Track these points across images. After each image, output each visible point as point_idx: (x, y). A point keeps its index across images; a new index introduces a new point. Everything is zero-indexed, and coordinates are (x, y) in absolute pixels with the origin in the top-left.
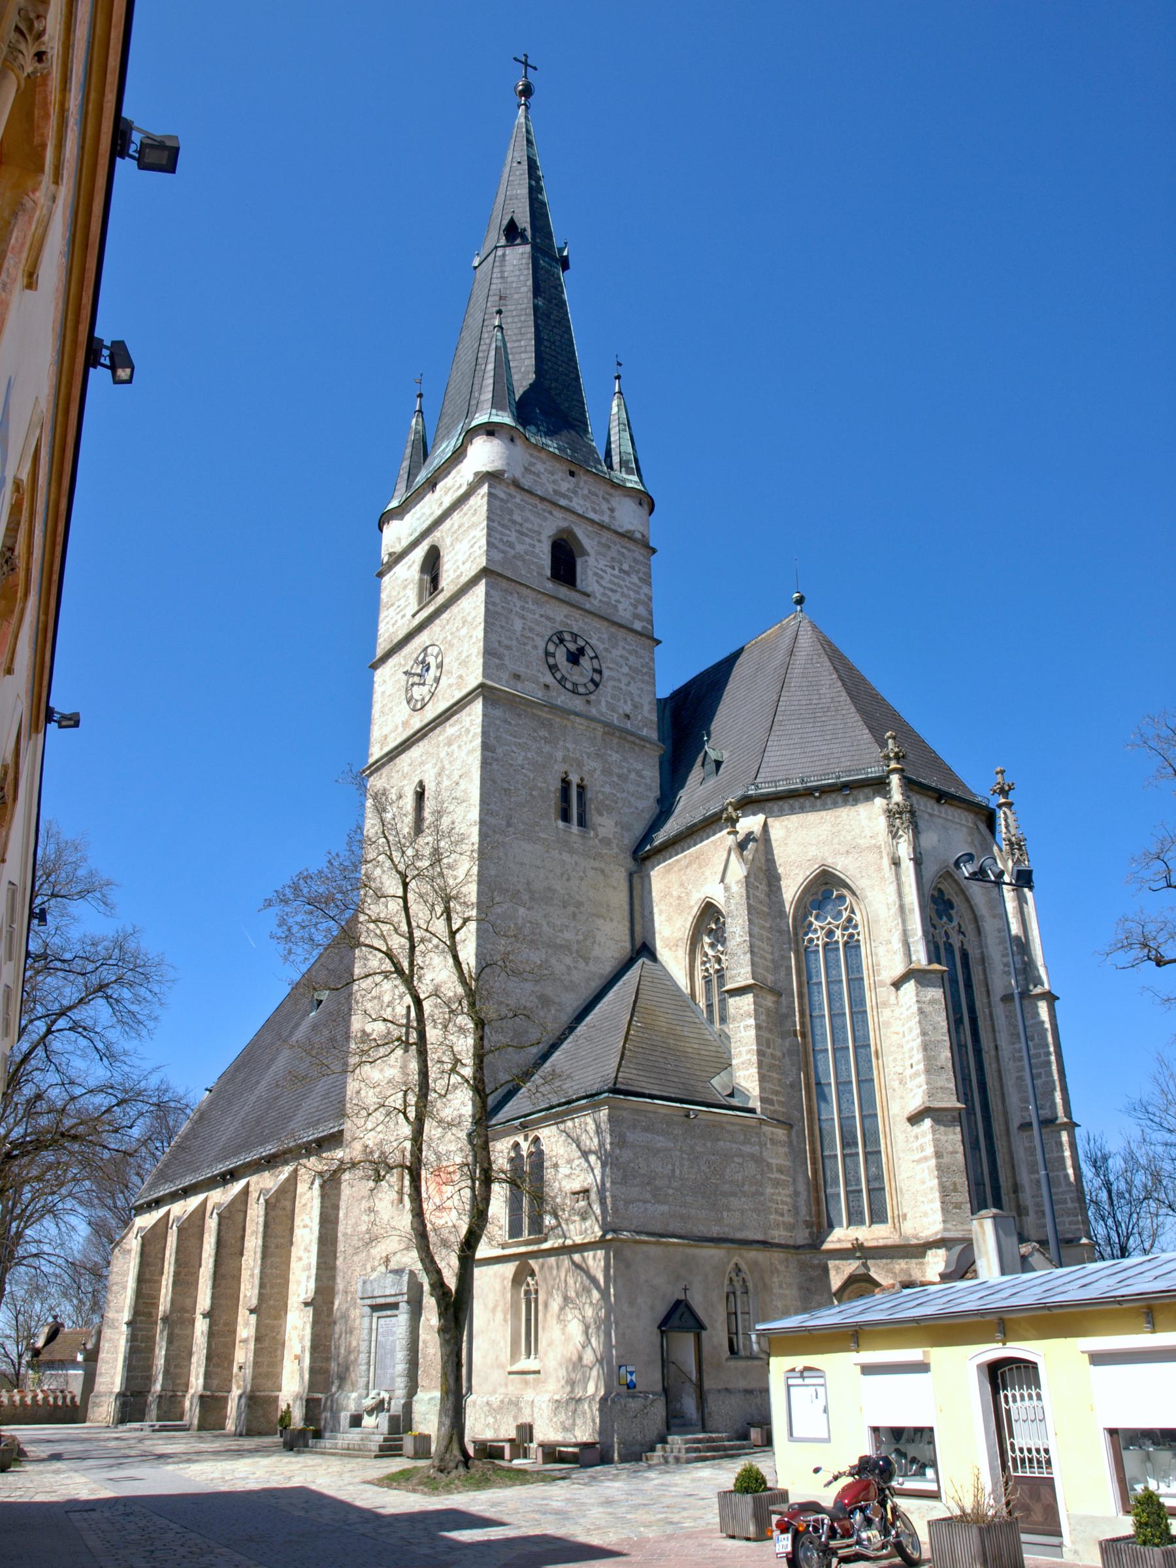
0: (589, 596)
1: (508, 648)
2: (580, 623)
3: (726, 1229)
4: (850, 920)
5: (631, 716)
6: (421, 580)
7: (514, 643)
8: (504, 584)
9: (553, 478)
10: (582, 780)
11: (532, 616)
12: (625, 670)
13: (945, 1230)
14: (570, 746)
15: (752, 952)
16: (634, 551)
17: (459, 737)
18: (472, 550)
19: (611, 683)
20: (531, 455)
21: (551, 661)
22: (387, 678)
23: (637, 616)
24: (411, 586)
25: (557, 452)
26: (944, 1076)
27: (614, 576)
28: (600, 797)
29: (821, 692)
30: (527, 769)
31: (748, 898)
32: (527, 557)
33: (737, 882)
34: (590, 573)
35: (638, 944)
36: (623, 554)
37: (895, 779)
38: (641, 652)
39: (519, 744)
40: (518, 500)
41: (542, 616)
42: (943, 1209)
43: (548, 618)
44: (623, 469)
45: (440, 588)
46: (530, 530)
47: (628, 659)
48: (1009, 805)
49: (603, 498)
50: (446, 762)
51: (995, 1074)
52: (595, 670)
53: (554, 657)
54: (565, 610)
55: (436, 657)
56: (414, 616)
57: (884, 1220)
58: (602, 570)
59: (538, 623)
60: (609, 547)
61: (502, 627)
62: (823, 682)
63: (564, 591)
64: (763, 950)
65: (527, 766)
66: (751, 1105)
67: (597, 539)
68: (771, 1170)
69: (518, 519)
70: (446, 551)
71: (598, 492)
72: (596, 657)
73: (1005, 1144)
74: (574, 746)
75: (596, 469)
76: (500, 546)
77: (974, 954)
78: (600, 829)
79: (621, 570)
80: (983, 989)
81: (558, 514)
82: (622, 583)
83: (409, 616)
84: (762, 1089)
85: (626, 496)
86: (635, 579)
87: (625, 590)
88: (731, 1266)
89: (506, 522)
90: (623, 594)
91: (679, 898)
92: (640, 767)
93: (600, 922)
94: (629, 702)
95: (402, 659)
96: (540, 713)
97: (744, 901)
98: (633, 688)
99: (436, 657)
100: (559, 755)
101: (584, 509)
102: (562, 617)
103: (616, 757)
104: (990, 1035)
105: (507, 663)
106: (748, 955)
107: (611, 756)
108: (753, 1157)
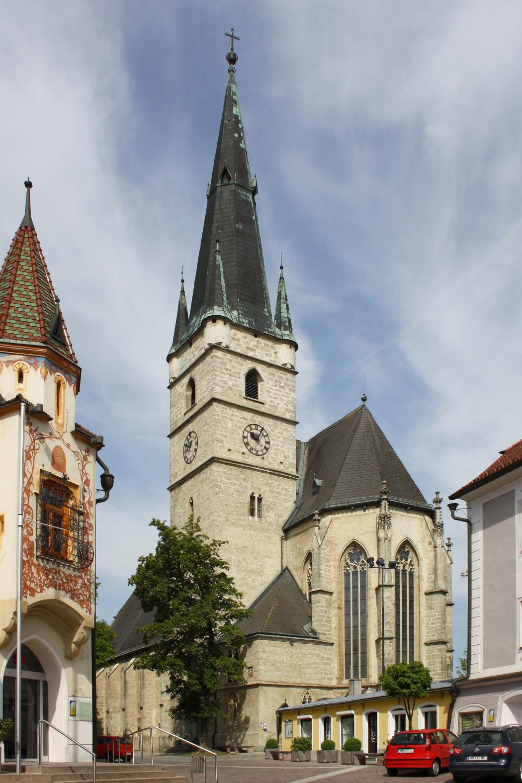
0: (263, 404)
1: (225, 436)
3: (304, 680)
5: (283, 462)
7: (228, 434)
10: (260, 496)
11: (236, 419)
12: (281, 439)
18: (208, 386)
19: (274, 447)
21: (246, 440)
22: (175, 444)
23: (288, 410)
24: (183, 398)
25: (248, 325)
27: (277, 390)
28: (268, 503)
29: (365, 453)
30: (236, 495)
32: (233, 388)
34: (264, 391)
35: (284, 568)
36: (281, 377)
39: (231, 483)
41: (241, 418)
43: (244, 418)
46: (235, 373)
51: (418, 623)
55: (195, 439)
56: (185, 414)
58: (270, 388)
59: (239, 422)
60: (274, 375)
61: (222, 426)
62: (366, 448)
63: (250, 404)
64: (326, 575)
65: (235, 493)
69: (228, 367)
70: (197, 383)
72: (267, 435)
73: (418, 649)
75: (268, 331)
76: (221, 384)
77: (416, 574)
78: (268, 518)
79: (281, 387)
80: (418, 589)
82: (280, 393)
83: (183, 414)
86: (287, 390)
89: (223, 370)
90: (281, 400)
93: (267, 559)
94: (283, 455)
95: (181, 436)
98: (285, 449)
99: (195, 439)
100: (249, 486)
103: (276, 483)
104: (418, 607)
105: (225, 444)
107: (273, 483)
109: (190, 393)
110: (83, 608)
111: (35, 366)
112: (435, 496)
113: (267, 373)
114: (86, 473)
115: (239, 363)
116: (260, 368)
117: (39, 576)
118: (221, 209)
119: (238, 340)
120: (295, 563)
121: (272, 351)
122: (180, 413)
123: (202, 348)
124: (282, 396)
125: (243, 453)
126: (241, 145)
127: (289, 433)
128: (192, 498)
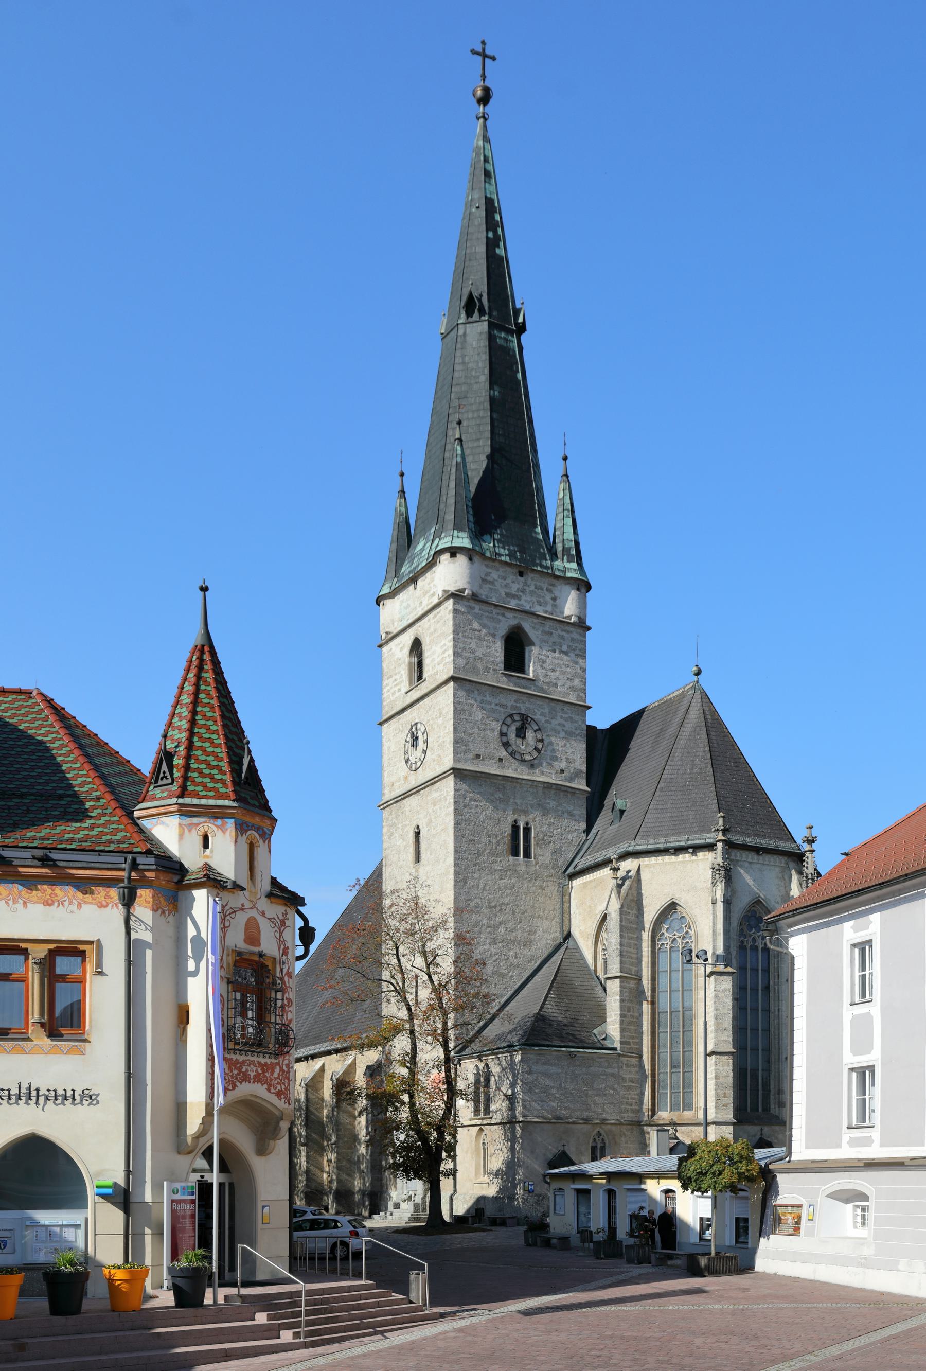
1: (471, 735)
2: (527, 705)
4: (687, 932)
6: (410, 664)
7: (476, 730)
8: (467, 685)
9: (505, 582)
11: (488, 706)
13: (716, 1117)
14: (518, 801)
15: (621, 955)
16: (571, 632)
17: (440, 800)
20: (487, 566)
26: (726, 1033)
27: (554, 658)
31: (621, 921)
33: (615, 911)
35: (565, 933)
36: (563, 637)
37: (720, 846)
38: (576, 718)
40: (477, 611)
41: (497, 704)
42: (716, 1107)
43: (502, 705)
44: (565, 558)
45: (424, 678)
47: (564, 726)
48: (812, 851)
49: (547, 590)
50: (433, 817)
52: (538, 740)
53: (506, 736)
54: (515, 696)
57: (691, 1109)
60: (551, 633)
64: (630, 952)
66: (615, 1046)
67: (541, 629)
68: (625, 1082)
71: (542, 585)
74: (521, 801)
75: (542, 566)
81: (509, 615)
84: (621, 1036)
85: (566, 584)
87: (564, 668)
88: (595, 1132)
91: (590, 907)
92: (571, 808)
96: (496, 781)
97: (618, 924)
101: (531, 604)
102: (513, 703)
106: (619, 958)
107: (549, 803)
108: (613, 1075)
109: (415, 660)
110: (280, 1099)
111: (222, 828)
112: (806, 833)
113: (540, 632)
114: (284, 941)
115: (493, 618)
116: (527, 626)
117: (231, 1071)
118: (463, 363)
119: (492, 583)
120: (582, 928)
121: (548, 597)
122: (399, 690)
123: (433, 595)
124: (563, 667)
125: (501, 760)
126: (497, 251)
127: (576, 724)
128: (418, 827)
